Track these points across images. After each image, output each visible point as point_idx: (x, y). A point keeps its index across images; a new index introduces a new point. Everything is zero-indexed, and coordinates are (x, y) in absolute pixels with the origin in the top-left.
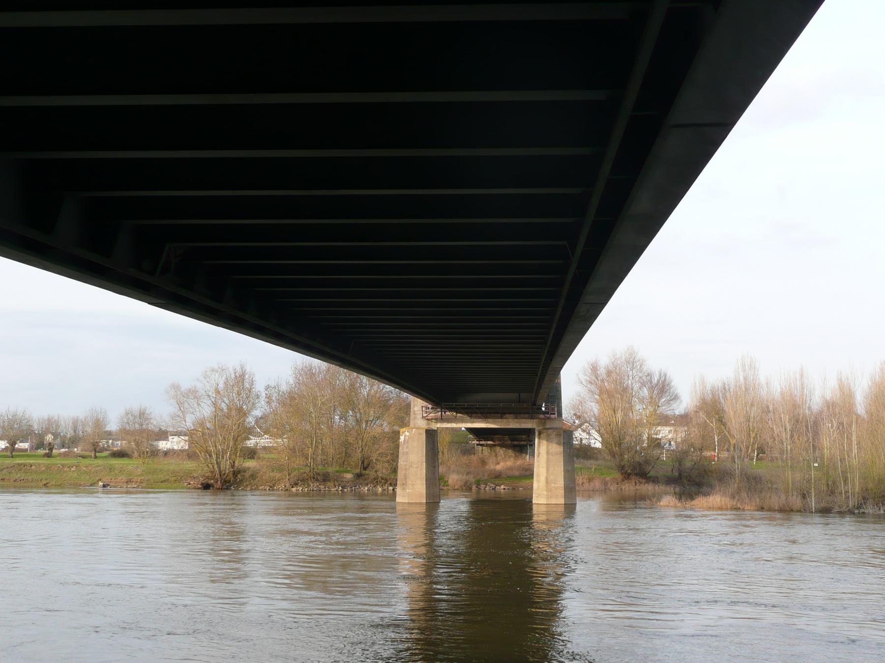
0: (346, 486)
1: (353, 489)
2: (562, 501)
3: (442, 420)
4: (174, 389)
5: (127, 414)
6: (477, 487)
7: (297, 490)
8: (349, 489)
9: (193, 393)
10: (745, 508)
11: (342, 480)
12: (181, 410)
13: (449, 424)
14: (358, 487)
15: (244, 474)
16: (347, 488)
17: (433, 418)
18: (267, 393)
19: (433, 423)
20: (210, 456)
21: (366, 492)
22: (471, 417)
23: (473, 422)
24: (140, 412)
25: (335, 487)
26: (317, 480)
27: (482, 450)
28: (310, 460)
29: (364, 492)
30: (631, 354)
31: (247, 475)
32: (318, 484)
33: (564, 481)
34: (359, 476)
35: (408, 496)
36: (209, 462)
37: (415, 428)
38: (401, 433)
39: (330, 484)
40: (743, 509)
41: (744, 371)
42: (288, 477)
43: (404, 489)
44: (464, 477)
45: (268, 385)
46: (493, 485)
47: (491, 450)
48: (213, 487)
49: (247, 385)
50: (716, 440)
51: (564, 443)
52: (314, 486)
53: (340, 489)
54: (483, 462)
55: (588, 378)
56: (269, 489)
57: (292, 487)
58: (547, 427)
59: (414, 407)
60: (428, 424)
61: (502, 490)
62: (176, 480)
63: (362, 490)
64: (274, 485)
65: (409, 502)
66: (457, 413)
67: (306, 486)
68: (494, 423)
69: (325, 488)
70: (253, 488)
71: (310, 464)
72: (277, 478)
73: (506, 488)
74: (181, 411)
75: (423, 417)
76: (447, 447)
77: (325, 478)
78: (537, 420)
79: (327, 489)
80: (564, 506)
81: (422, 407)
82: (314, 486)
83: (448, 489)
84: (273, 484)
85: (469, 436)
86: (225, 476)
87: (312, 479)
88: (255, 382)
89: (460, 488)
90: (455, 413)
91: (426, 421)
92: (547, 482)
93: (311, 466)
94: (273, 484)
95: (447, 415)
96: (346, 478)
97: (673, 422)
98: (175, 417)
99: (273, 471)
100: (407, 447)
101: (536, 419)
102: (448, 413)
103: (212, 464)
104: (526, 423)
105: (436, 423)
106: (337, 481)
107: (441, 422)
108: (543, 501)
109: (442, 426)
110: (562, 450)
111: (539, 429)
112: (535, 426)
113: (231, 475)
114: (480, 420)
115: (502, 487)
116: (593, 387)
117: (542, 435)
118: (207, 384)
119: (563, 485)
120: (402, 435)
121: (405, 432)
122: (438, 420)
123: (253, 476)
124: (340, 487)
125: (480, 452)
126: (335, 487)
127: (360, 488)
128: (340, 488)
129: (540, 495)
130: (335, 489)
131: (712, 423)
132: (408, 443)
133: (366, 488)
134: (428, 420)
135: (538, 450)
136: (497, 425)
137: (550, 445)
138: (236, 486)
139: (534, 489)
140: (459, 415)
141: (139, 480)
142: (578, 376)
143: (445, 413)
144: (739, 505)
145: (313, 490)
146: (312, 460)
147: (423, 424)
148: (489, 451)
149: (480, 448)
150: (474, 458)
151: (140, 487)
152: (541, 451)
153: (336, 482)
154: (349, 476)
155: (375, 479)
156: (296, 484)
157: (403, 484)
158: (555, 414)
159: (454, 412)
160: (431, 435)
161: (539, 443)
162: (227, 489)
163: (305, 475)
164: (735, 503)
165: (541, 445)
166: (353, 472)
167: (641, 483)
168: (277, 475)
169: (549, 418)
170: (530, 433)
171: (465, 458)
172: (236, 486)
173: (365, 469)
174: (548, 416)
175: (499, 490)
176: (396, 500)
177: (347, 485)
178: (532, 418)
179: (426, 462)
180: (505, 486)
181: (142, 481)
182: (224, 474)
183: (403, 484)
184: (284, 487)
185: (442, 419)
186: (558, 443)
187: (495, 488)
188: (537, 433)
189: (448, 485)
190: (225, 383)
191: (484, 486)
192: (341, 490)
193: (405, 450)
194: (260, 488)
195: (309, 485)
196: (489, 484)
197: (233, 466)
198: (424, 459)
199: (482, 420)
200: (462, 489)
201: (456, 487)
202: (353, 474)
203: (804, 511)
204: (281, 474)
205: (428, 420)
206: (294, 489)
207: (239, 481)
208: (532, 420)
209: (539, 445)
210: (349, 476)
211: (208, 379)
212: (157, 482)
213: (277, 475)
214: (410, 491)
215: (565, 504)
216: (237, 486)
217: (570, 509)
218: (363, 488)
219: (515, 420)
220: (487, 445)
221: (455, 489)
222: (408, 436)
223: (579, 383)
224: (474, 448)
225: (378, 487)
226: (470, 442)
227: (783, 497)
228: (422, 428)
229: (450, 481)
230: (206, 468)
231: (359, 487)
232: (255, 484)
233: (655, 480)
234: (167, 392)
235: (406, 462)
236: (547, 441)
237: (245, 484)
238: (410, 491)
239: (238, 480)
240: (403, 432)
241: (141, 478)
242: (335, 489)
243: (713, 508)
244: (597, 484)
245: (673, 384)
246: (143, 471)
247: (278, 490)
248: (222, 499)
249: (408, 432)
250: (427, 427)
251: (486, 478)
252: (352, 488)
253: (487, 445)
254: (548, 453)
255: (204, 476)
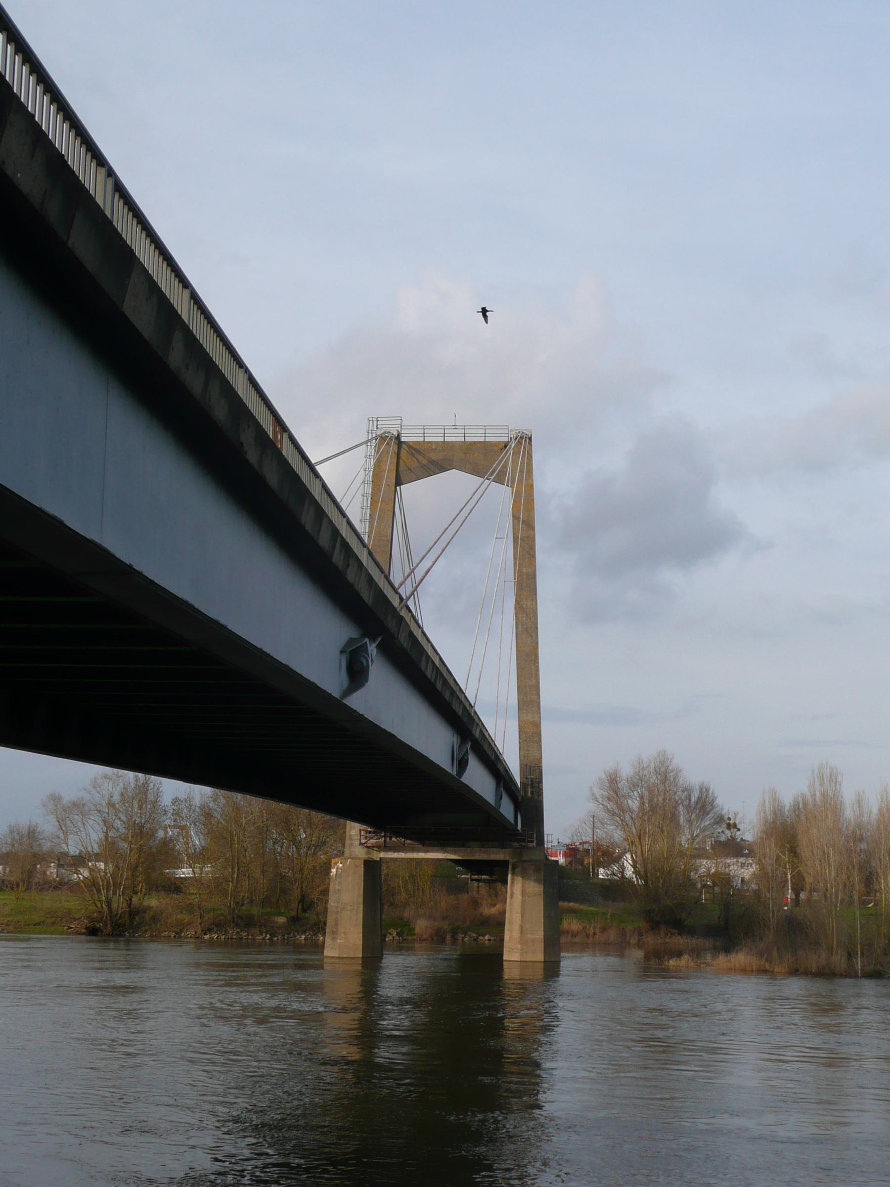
0: (277, 933)
1: (286, 937)
2: (540, 957)
3: (385, 847)
4: (54, 801)
5: (12, 832)
6: (452, 937)
7: (210, 938)
8: (280, 937)
9: (78, 806)
10: (775, 970)
11: (272, 925)
12: (62, 829)
13: (396, 854)
14: (292, 935)
15: (143, 915)
16: (277, 937)
17: (374, 845)
18: (175, 808)
19: (375, 852)
20: (99, 891)
21: (303, 942)
22: (423, 845)
23: (427, 851)
24: (29, 830)
25: (262, 935)
26: (237, 925)
27: (478, 887)
28: (229, 898)
29: (301, 941)
30: (662, 763)
31: (147, 917)
32: (238, 930)
33: (544, 931)
34: (294, 920)
35: (339, 949)
36: (97, 899)
37: (351, 858)
38: (332, 865)
39: (256, 930)
40: (772, 972)
41: (822, 784)
42: (199, 920)
43: (334, 939)
44: (436, 924)
45: (176, 798)
46: (474, 935)
47: (490, 888)
48: (102, 932)
49: (151, 797)
50: (789, 877)
51: (545, 881)
52: (232, 932)
53: (267, 938)
54: (476, 904)
55: (605, 794)
56: (175, 937)
57: (205, 934)
58: (524, 859)
59: (350, 830)
60: (368, 853)
61: (487, 942)
62: (54, 923)
63: (298, 939)
64: (181, 931)
65: (341, 956)
66: (406, 838)
67: (223, 933)
68: (455, 853)
69: (248, 935)
70: (154, 934)
71: (230, 904)
72: (185, 921)
73: (492, 938)
74: (61, 831)
75: (361, 844)
76: (429, 883)
77: (248, 922)
78: (512, 849)
79: (250, 937)
80: (543, 964)
81: (360, 830)
82: (233, 933)
83: (414, 939)
84: (180, 930)
85: (457, 868)
86: (117, 918)
87: (232, 923)
88: (162, 794)
89: (430, 938)
90: (403, 840)
91: (365, 850)
92: (522, 932)
93: (230, 906)
94: (180, 930)
95: (393, 841)
96: (277, 922)
97: (747, 851)
98: (53, 838)
99: (181, 912)
100: (339, 884)
101: (510, 848)
102: (394, 839)
103: (99, 901)
104: (496, 854)
105: (379, 851)
106: (265, 927)
107: (384, 851)
108: (515, 957)
109: (386, 856)
110: (542, 889)
111: (514, 861)
112: (507, 858)
113: (127, 916)
114: (436, 848)
115: (487, 937)
116: (610, 805)
117: (516, 870)
118: (98, 795)
119: (542, 937)
120: (334, 868)
121: (338, 862)
122: (382, 848)
123: (155, 919)
124: (268, 935)
125: (475, 888)
126: (262, 935)
127: (295, 937)
128: (268, 936)
129: (512, 949)
130: (261, 937)
131: (785, 855)
132: (340, 877)
133: (303, 937)
134: (368, 847)
135: (512, 890)
136: (459, 856)
137: (527, 882)
138: (131, 931)
139: (505, 941)
140: (408, 841)
141: (6, 921)
142: (591, 790)
143: (390, 839)
144: (768, 967)
145: (232, 938)
146: (232, 898)
147: (361, 853)
148: (487, 888)
149: (475, 884)
150: (464, 897)
151: (5, 931)
152: (515, 891)
153: (263, 927)
154: (281, 920)
155: (316, 924)
156: (210, 930)
157: (333, 932)
158: (533, 842)
159: (403, 838)
160: (372, 868)
161: (513, 879)
162: (120, 935)
163: (222, 918)
164: (762, 963)
165: (515, 883)
166: (287, 915)
167: (672, 934)
168: (186, 918)
169: (526, 848)
170: (503, 866)
171: (452, 897)
172: (131, 931)
173: (305, 911)
174: (523, 844)
175: (482, 941)
176: (323, 952)
177: (278, 932)
178: (464, 846)
179: (363, 904)
180: (490, 936)
181: (9, 923)
182: (116, 915)
183: (333, 932)
184: (194, 933)
185: (385, 846)
186: (538, 881)
187: (477, 938)
188: (510, 867)
189: (414, 934)
190: (122, 795)
191: (463, 936)
192: (269, 939)
193: (337, 887)
194: (163, 935)
195: (226, 932)
196: (469, 933)
197: (129, 905)
198: (361, 900)
199: (438, 848)
200: (432, 940)
201: (425, 937)
202: (287, 917)
203: (850, 974)
204: (192, 916)
205: (368, 847)
206: (207, 937)
207: (136, 925)
208: (504, 850)
209: (512, 883)
210: (281, 920)
211: (98, 789)
212: (29, 925)
213: (186, 918)
214: (341, 941)
215: (544, 962)
216: (133, 932)
217: (551, 969)
218: (298, 937)
219: (482, 849)
220: (484, 881)
221: (423, 940)
222: (341, 869)
223: (593, 800)
224: (468, 883)
225: (320, 935)
226: (459, 876)
227: (824, 955)
228: (359, 859)
229: (417, 930)
230: (92, 907)
231: (294, 934)
232: (156, 930)
233: (691, 931)
234: (44, 806)
235: (338, 903)
236: (523, 878)
237: (143, 929)
238: (341, 941)
239: (135, 923)
240: (336, 863)
241: (8, 919)
242: (261, 937)
243: (735, 969)
244: (612, 935)
245: (717, 801)
246: (12, 910)
247: (186, 937)
248: (113, 952)
249: (341, 863)
250: (367, 856)
251: (468, 924)
252: (284, 936)
253: (484, 881)
254: (523, 893)
255: (89, 917)
